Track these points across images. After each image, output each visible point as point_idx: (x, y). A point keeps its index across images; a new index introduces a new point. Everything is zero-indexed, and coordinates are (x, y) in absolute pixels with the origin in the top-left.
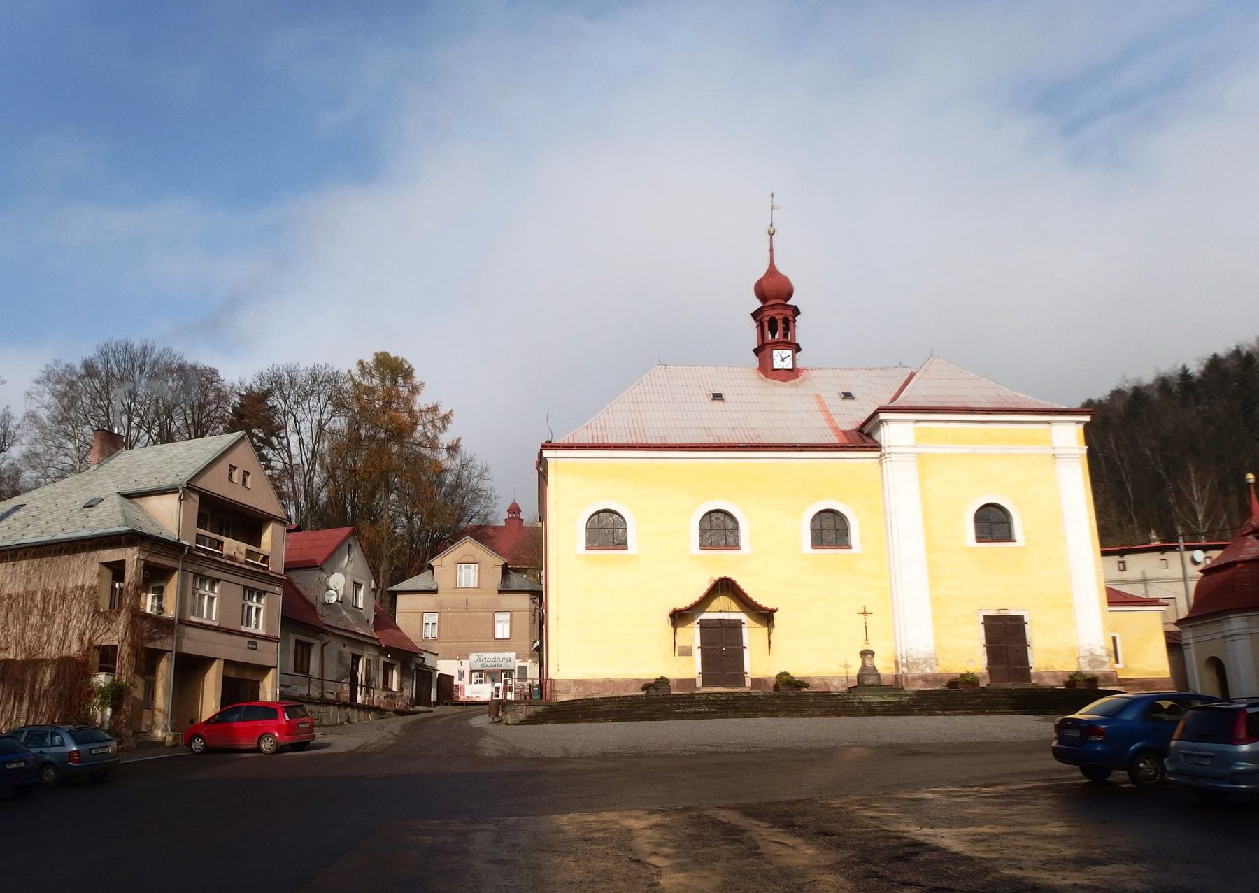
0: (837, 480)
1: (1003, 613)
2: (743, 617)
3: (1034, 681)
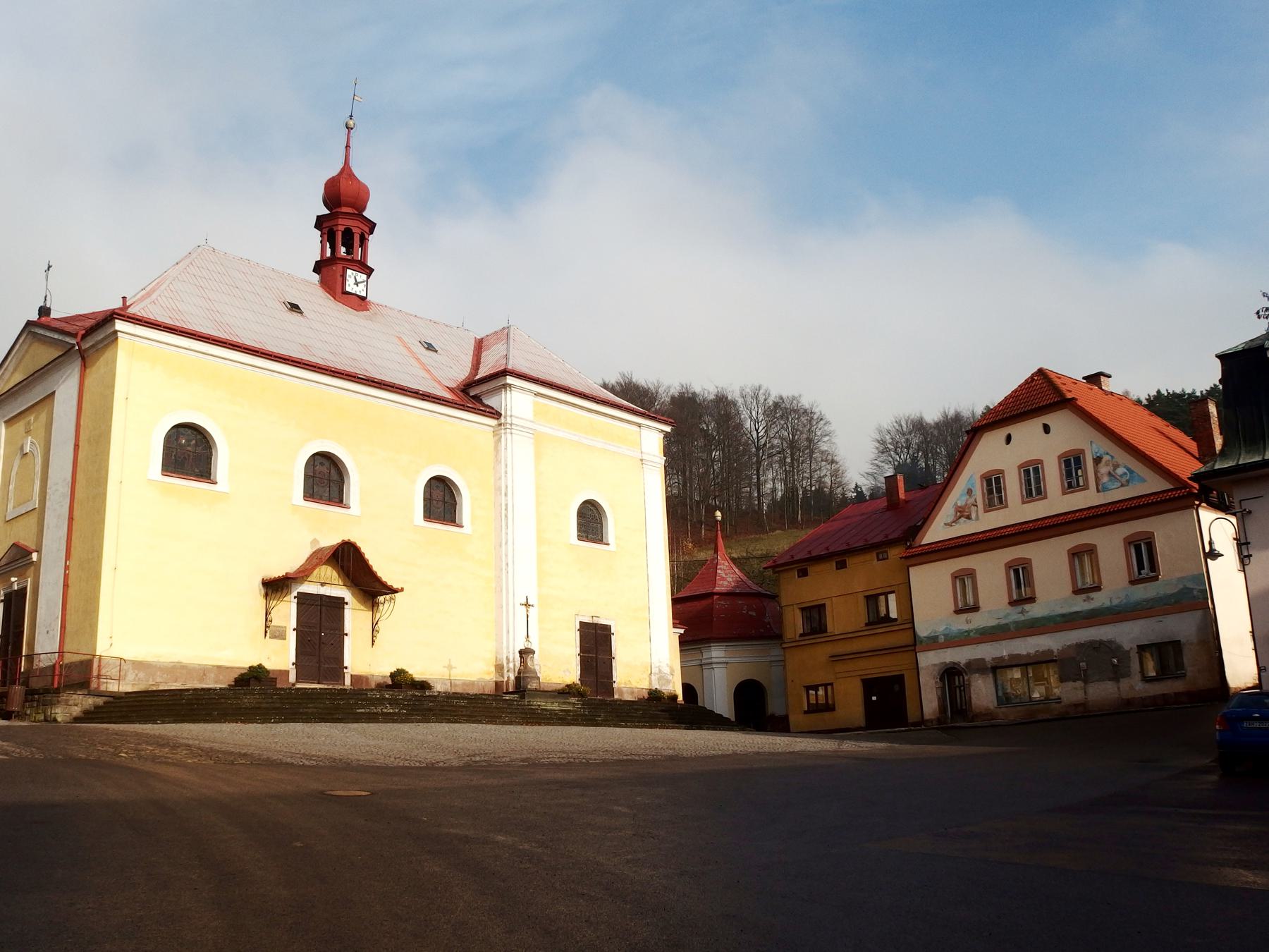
0: (454, 442)
1: (595, 621)
3: (616, 697)
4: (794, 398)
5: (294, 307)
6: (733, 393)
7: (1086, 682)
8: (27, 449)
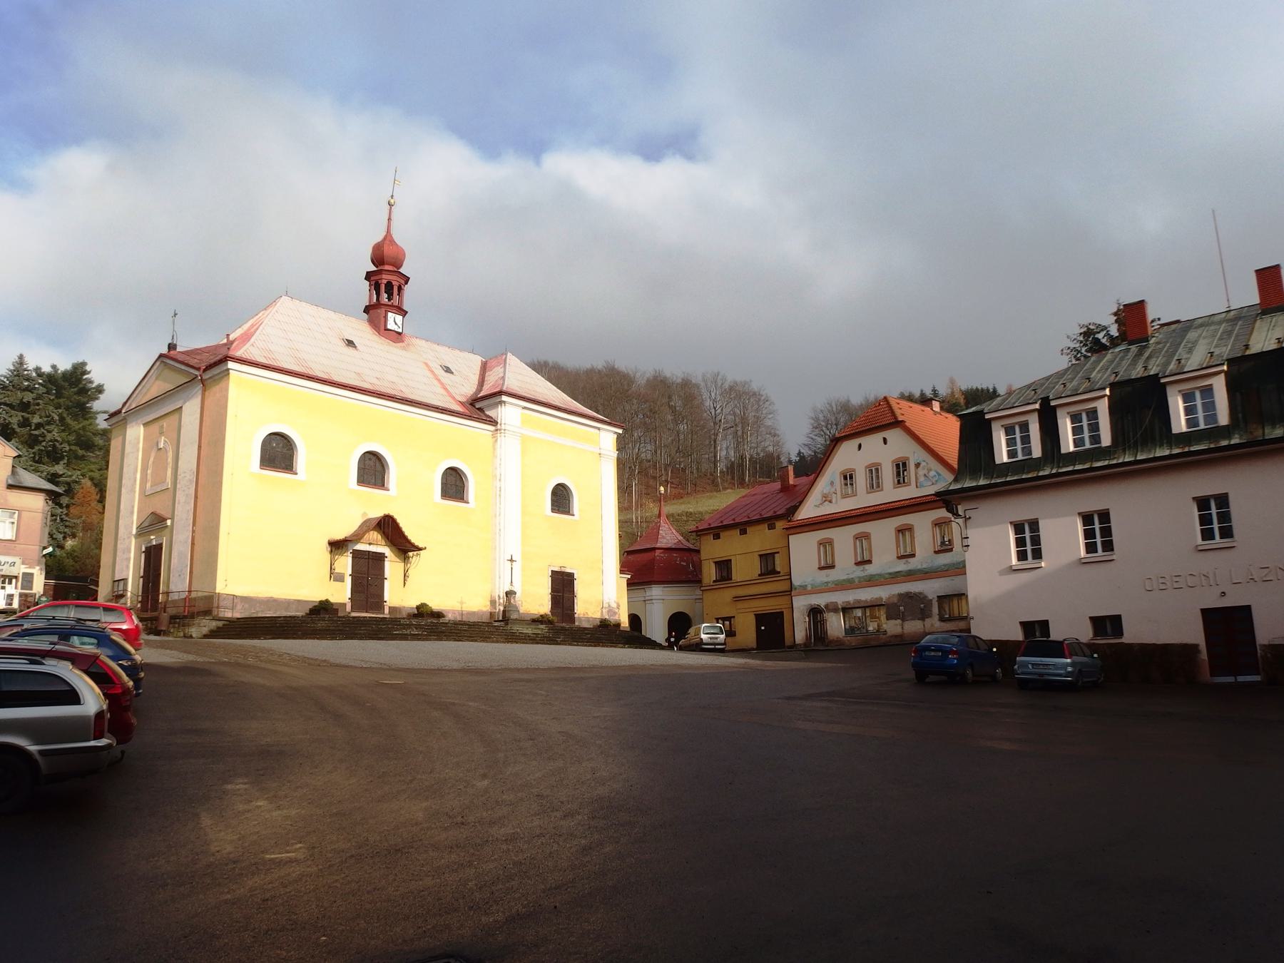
2: (386, 550)
4: (746, 383)
5: (350, 343)
6: (697, 378)
7: (903, 620)
8: (161, 445)
